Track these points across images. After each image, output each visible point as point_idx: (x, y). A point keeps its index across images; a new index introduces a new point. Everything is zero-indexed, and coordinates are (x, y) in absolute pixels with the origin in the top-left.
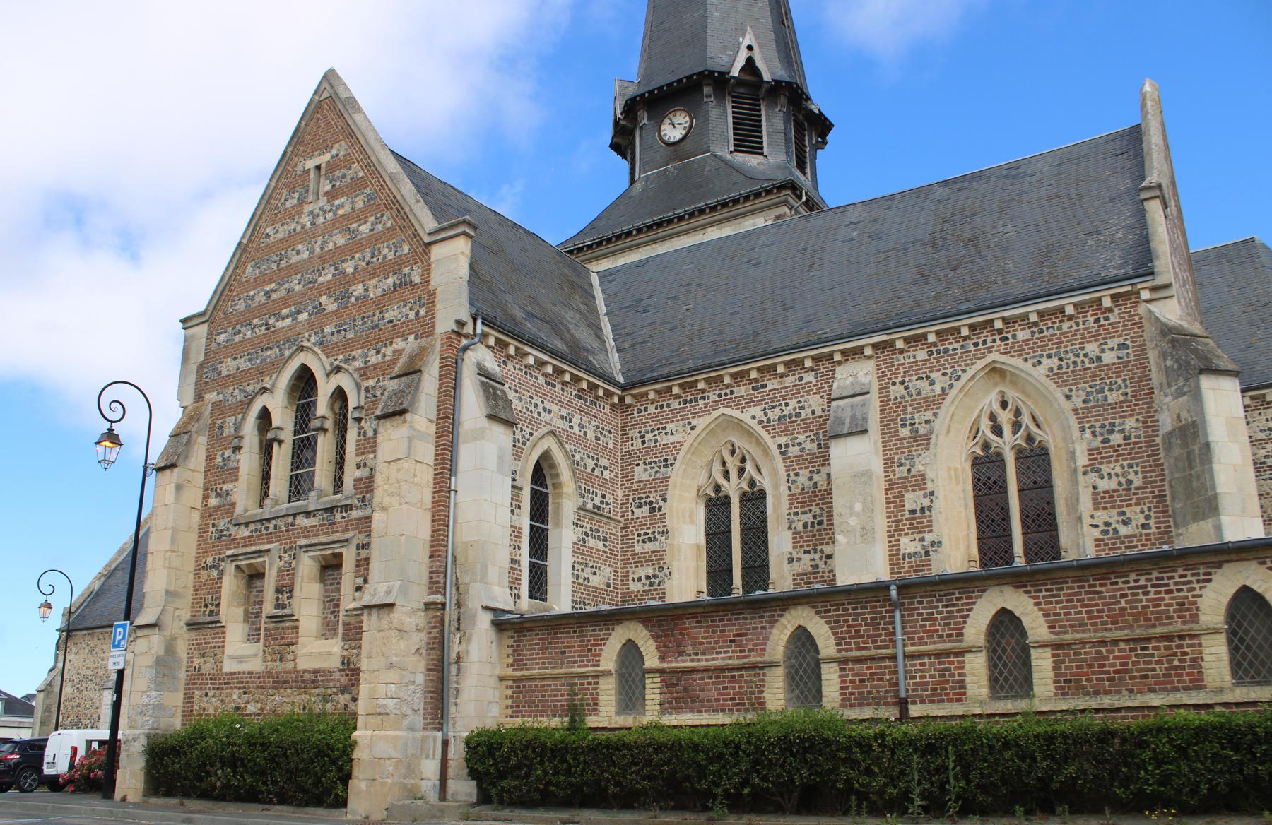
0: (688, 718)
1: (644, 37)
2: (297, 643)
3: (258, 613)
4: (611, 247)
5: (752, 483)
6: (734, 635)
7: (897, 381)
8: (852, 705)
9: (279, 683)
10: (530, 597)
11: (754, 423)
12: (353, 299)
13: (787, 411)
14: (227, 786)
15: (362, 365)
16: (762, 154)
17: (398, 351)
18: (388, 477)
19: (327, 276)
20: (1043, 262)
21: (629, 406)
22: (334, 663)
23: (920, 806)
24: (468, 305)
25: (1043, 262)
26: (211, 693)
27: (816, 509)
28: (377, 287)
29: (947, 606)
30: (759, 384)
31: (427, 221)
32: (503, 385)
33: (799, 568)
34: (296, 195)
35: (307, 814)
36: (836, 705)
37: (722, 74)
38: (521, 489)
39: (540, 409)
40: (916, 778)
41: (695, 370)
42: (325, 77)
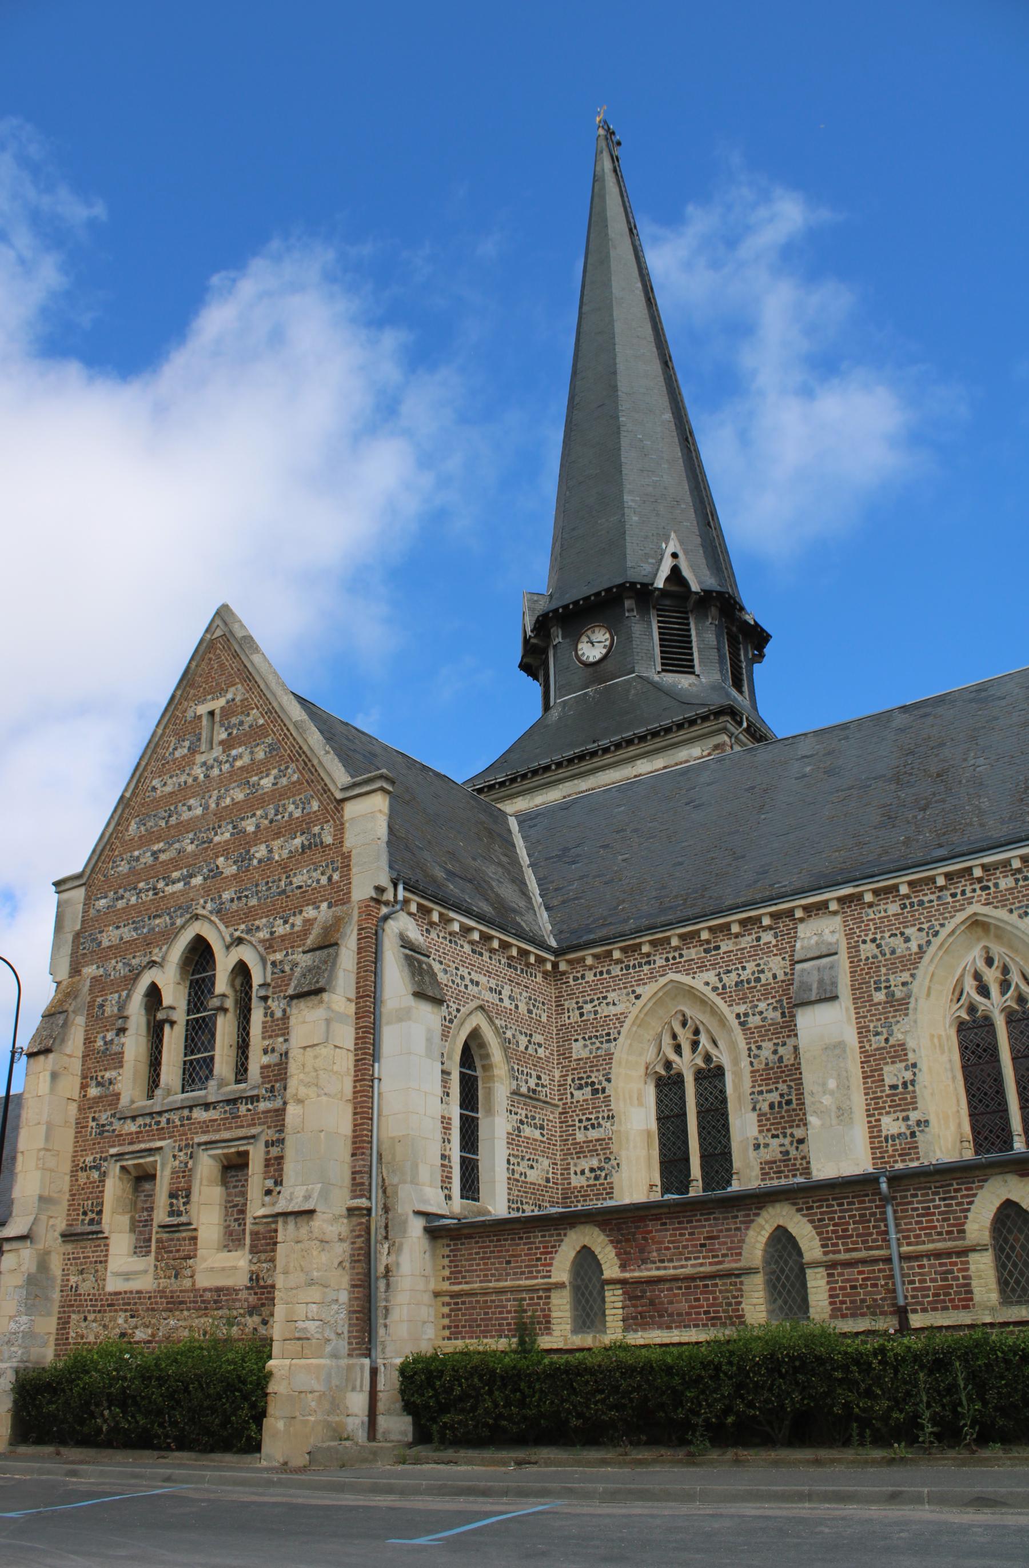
0: (657, 1336)
1: (554, 544)
2: (195, 1256)
3: (146, 1221)
4: (527, 784)
5: (708, 1058)
6: (705, 1238)
7: (868, 939)
8: (844, 1316)
9: (174, 1303)
10: (462, 1197)
11: (707, 990)
12: (255, 862)
13: (745, 975)
14: (115, 1429)
15: (268, 936)
16: (693, 673)
17: (309, 920)
18: (303, 1065)
19: (224, 836)
20: (1022, 800)
21: (564, 973)
22: (241, 1280)
23: (931, 1433)
24: (387, 869)
25: (1022, 800)
26: (91, 1317)
27: (783, 1087)
28: (282, 849)
29: (944, 1199)
30: (712, 945)
31: (339, 775)
32: (429, 957)
33: (766, 1155)
34: (187, 744)
35: (213, 1461)
36: (826, 1316)
37: (644, 585)
38: (449, 1074)
39: (467, 982)
40: (925, 1399)
41: (639, 931)
42: (218, 613)
